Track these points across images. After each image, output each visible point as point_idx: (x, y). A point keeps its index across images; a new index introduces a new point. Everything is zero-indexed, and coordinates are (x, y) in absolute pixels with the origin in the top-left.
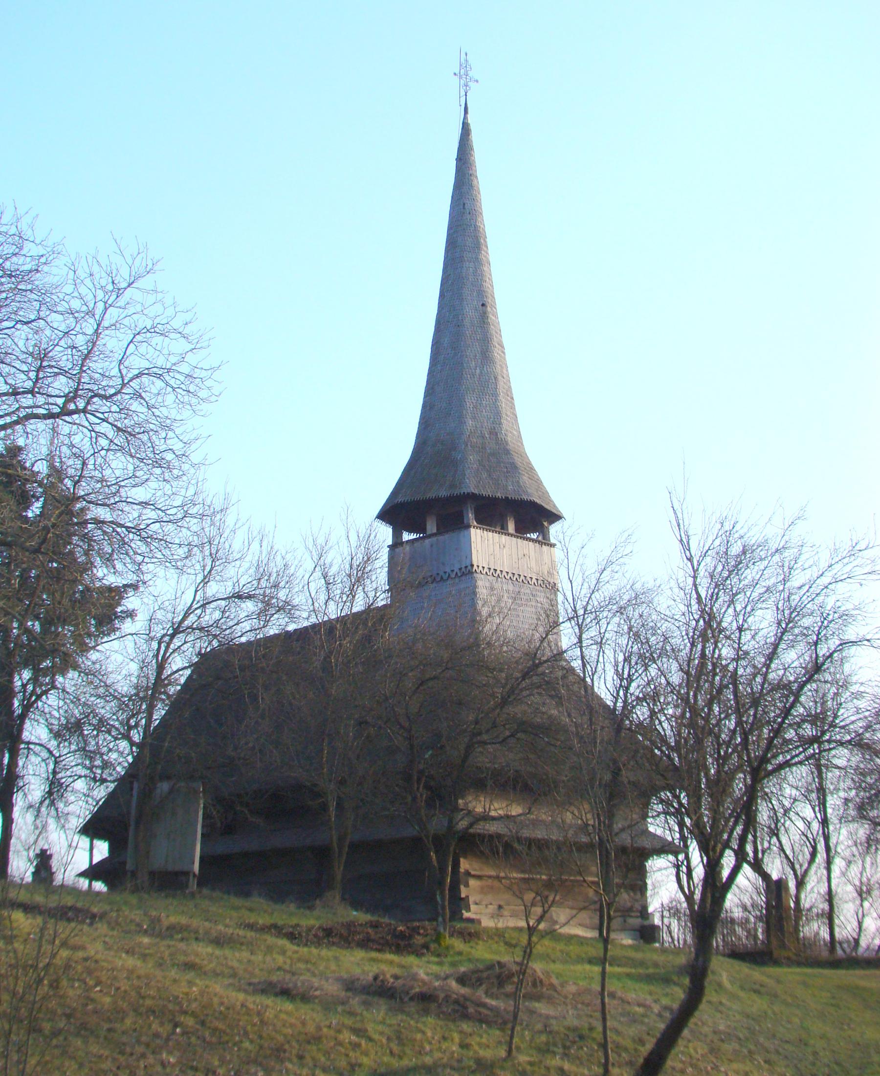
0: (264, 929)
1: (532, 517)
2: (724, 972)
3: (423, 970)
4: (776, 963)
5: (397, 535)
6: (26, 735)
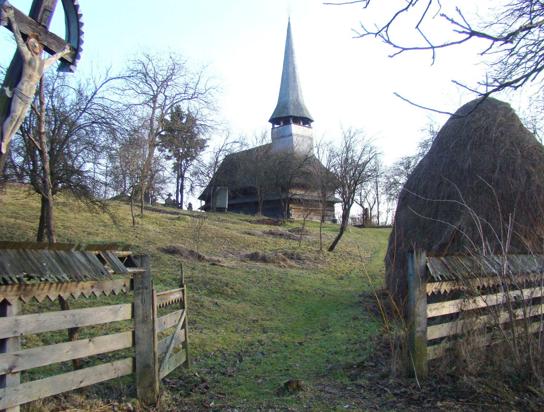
0: (243, 220)
1: (306, 121)
2: (350, 229)
3: (281, 229)
4: (365, 227)
5: (273, 125)
6: (185, 176)
